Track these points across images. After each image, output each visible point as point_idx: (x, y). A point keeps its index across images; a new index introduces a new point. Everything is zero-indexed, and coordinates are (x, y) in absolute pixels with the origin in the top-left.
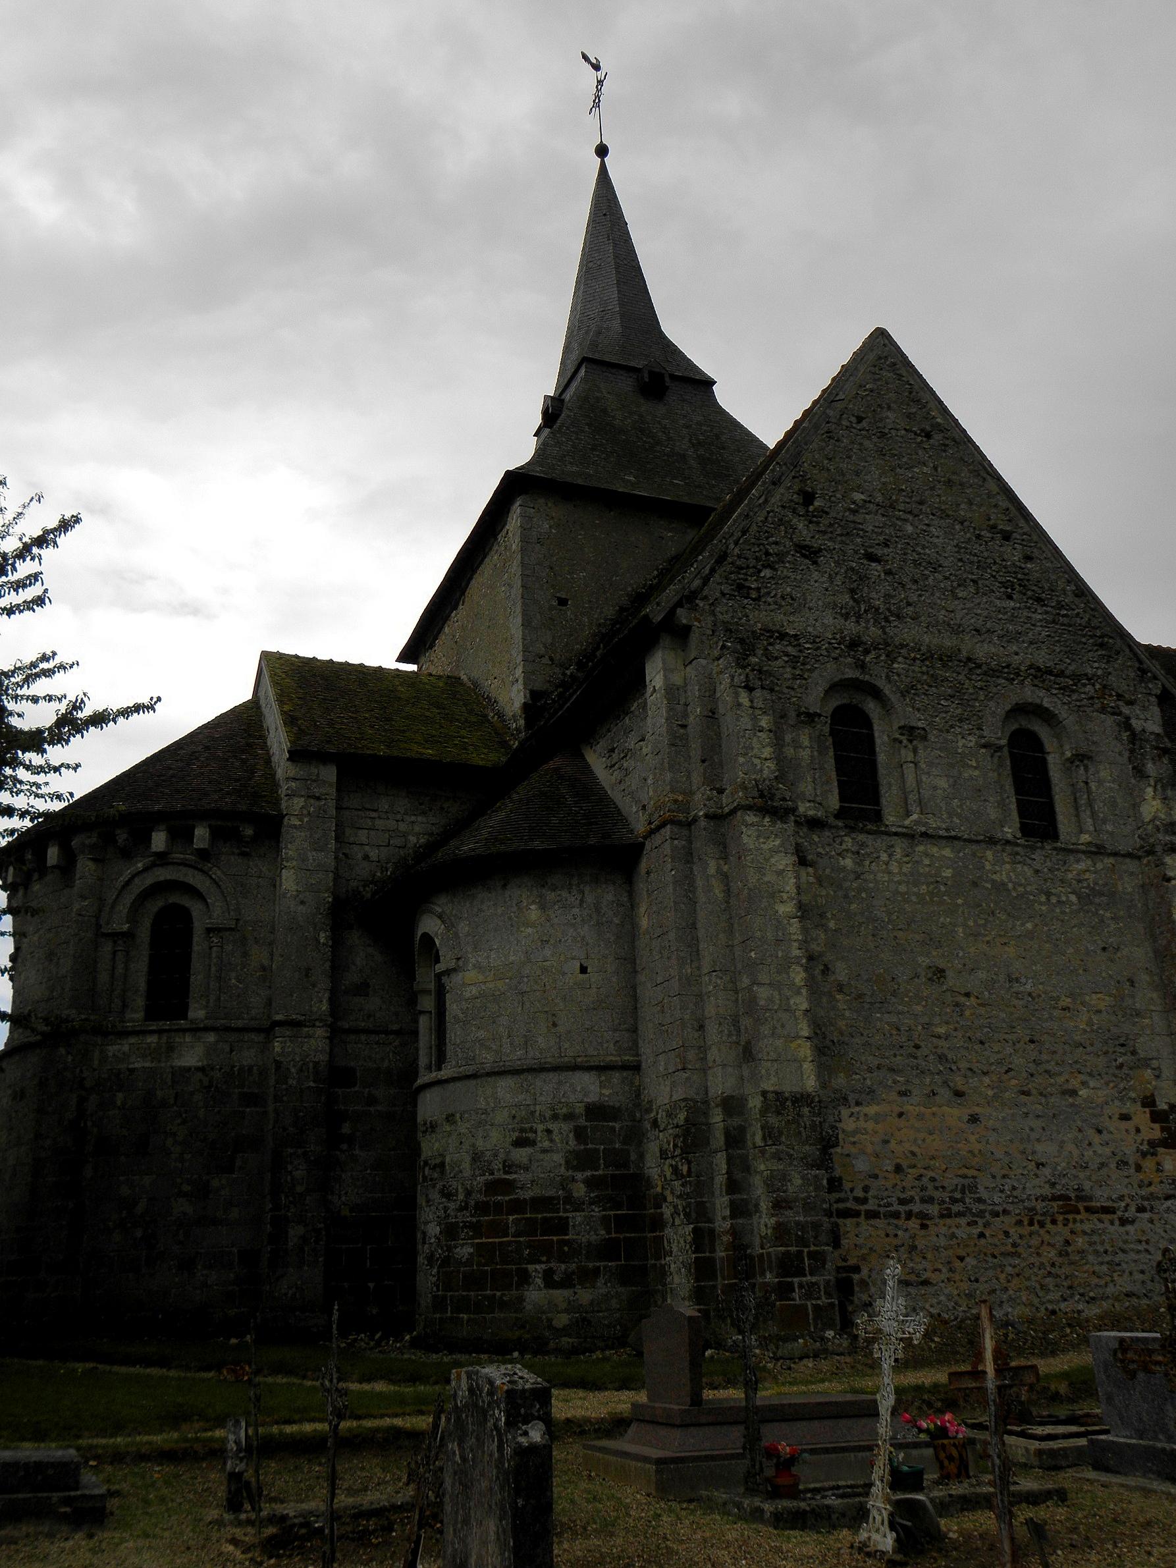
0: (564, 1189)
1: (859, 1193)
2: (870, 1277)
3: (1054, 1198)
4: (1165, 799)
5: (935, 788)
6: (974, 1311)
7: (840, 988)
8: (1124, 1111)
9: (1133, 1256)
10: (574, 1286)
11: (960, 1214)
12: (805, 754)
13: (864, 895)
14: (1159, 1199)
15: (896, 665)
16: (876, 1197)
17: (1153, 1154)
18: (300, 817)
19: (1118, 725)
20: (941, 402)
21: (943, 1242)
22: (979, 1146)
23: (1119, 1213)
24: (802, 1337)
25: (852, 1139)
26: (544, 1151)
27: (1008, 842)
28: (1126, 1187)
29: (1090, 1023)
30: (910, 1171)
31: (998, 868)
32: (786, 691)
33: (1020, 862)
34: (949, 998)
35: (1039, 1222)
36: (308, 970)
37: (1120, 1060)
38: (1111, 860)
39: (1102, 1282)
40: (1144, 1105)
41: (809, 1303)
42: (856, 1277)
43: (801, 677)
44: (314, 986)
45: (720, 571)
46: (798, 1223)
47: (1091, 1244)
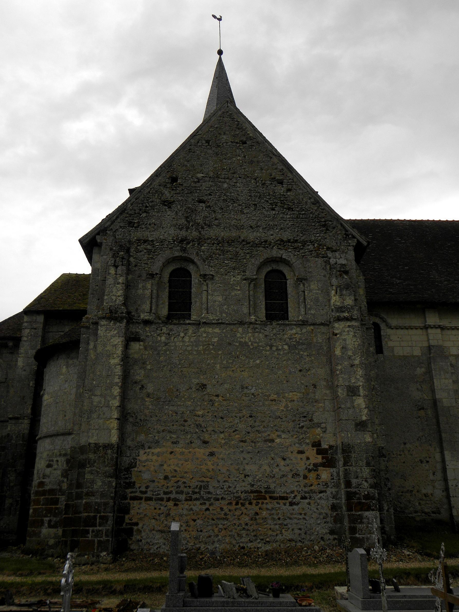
0: (59, 486)
1: (143, 489)
2: (142, 528)
3: (252, 492)
4: (341, 295)
5: (215, 301)
6: (197, 546)
7: (148, 395)
8: (300, 449)
9: (295, 521)
10: (58, 527)
11: (196, 499)
12: (148, 292)
13: (168, 353)
14: (316, 493)
15: (203, 248)
16: (152, 491)
17: (315, 470)
18: (27, 337)
19: (325, 262)
20: (253, 127)
21: (185, 512)
22: (212, 467)
23: (290, 500)
24: (88, 555)
25: (144, 464)
26: (55, 469)
27: (251, 323)
28: (297, 486)
29: (286, 407)
30: (173, 479)
31: (244, 336)
32: (143, 265)
33: (257, 332)
34: (206, 398)
35: (241, 503)
36: (24, 397)
37: (302, 424)
38: (312, 327)
39: (275, 534)
40: (313, 446)
41: (96, 540)
42: (135, 528)
43: (152, 258)
44: (26, 403)
45: (121, 217)
46: (96, 503)
47: (270, 515)
